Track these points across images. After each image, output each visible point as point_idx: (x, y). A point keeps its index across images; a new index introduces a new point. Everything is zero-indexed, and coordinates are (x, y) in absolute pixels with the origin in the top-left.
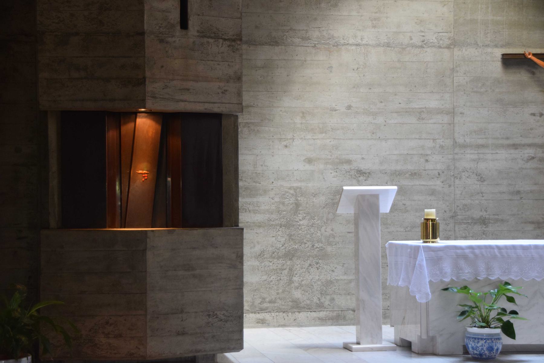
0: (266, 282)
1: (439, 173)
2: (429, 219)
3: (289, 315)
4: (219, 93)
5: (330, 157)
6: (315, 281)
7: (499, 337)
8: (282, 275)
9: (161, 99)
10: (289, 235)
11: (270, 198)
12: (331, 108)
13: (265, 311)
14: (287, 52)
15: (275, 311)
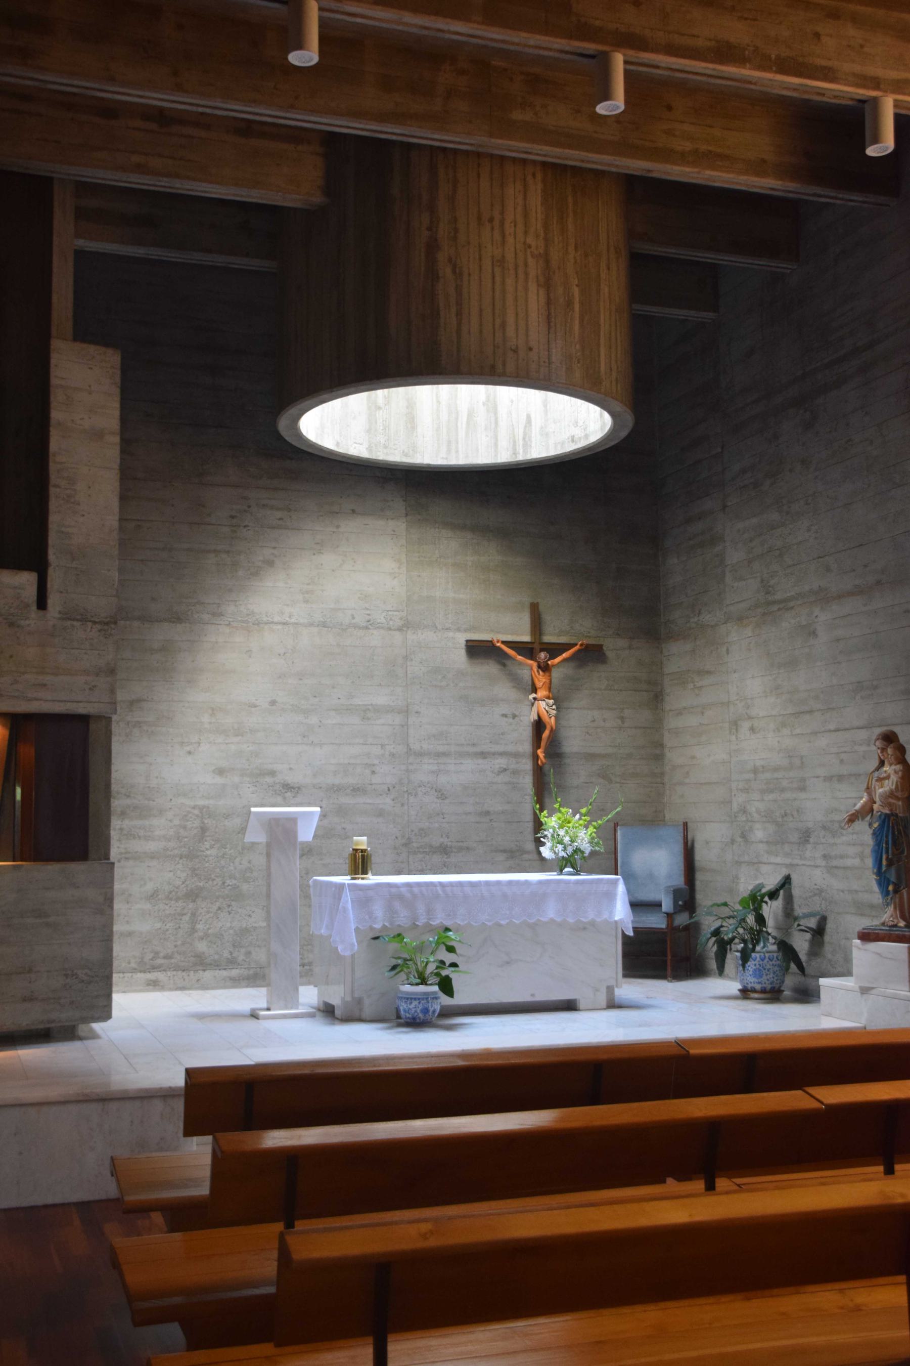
1: (389, 788)
2: (359, 850)
5: (248, 767)
6: (226, 929)
7: (437, 996)
13: (158, 970)
14: (192, 631)
15: (172, 969)
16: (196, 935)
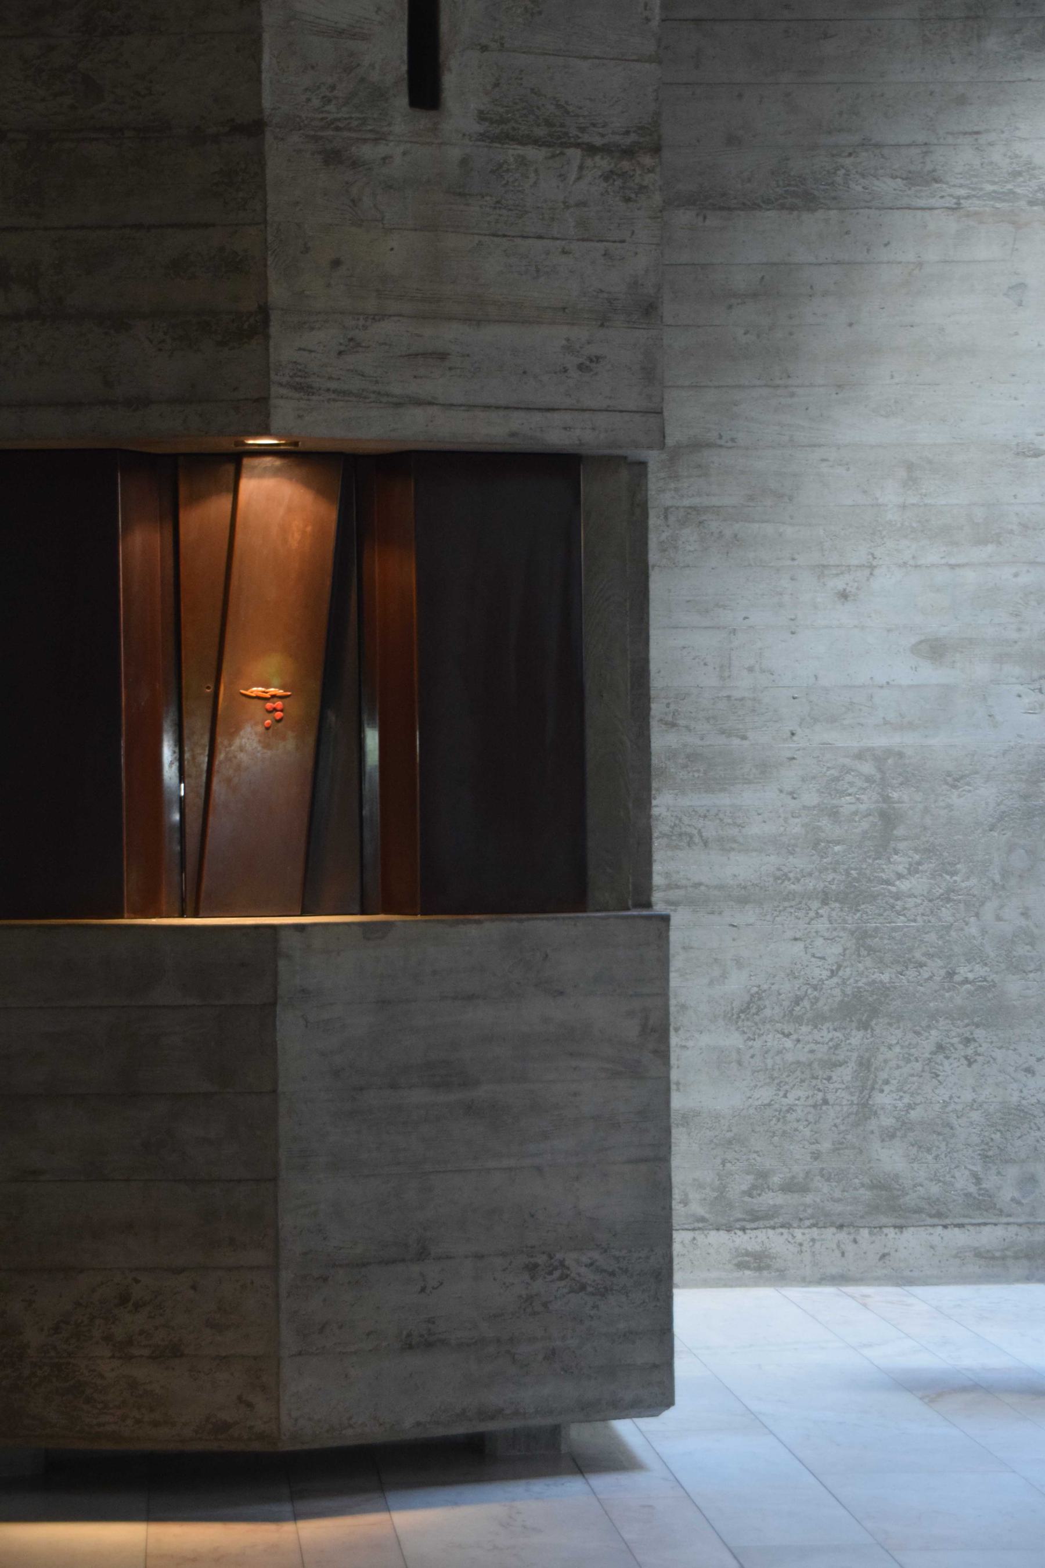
0: (769, 1112)
3: (858, 1238)
4: (565, 370)
5: (1015, 635)
8: (831, 1086)
9: (333, 396)
10: (855, 932)
11: (781, 791)
12: (1018, 445)
13: (767, 1223)
14: (847, 233)
15: (808, 1223)
16: (873, 1124)
